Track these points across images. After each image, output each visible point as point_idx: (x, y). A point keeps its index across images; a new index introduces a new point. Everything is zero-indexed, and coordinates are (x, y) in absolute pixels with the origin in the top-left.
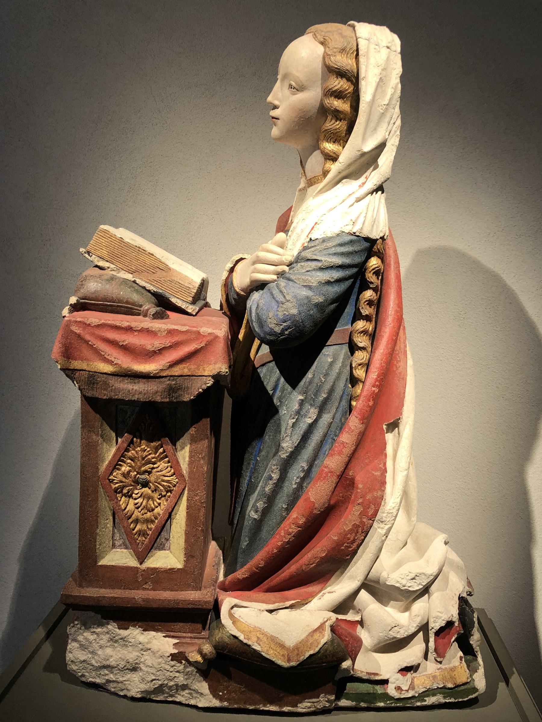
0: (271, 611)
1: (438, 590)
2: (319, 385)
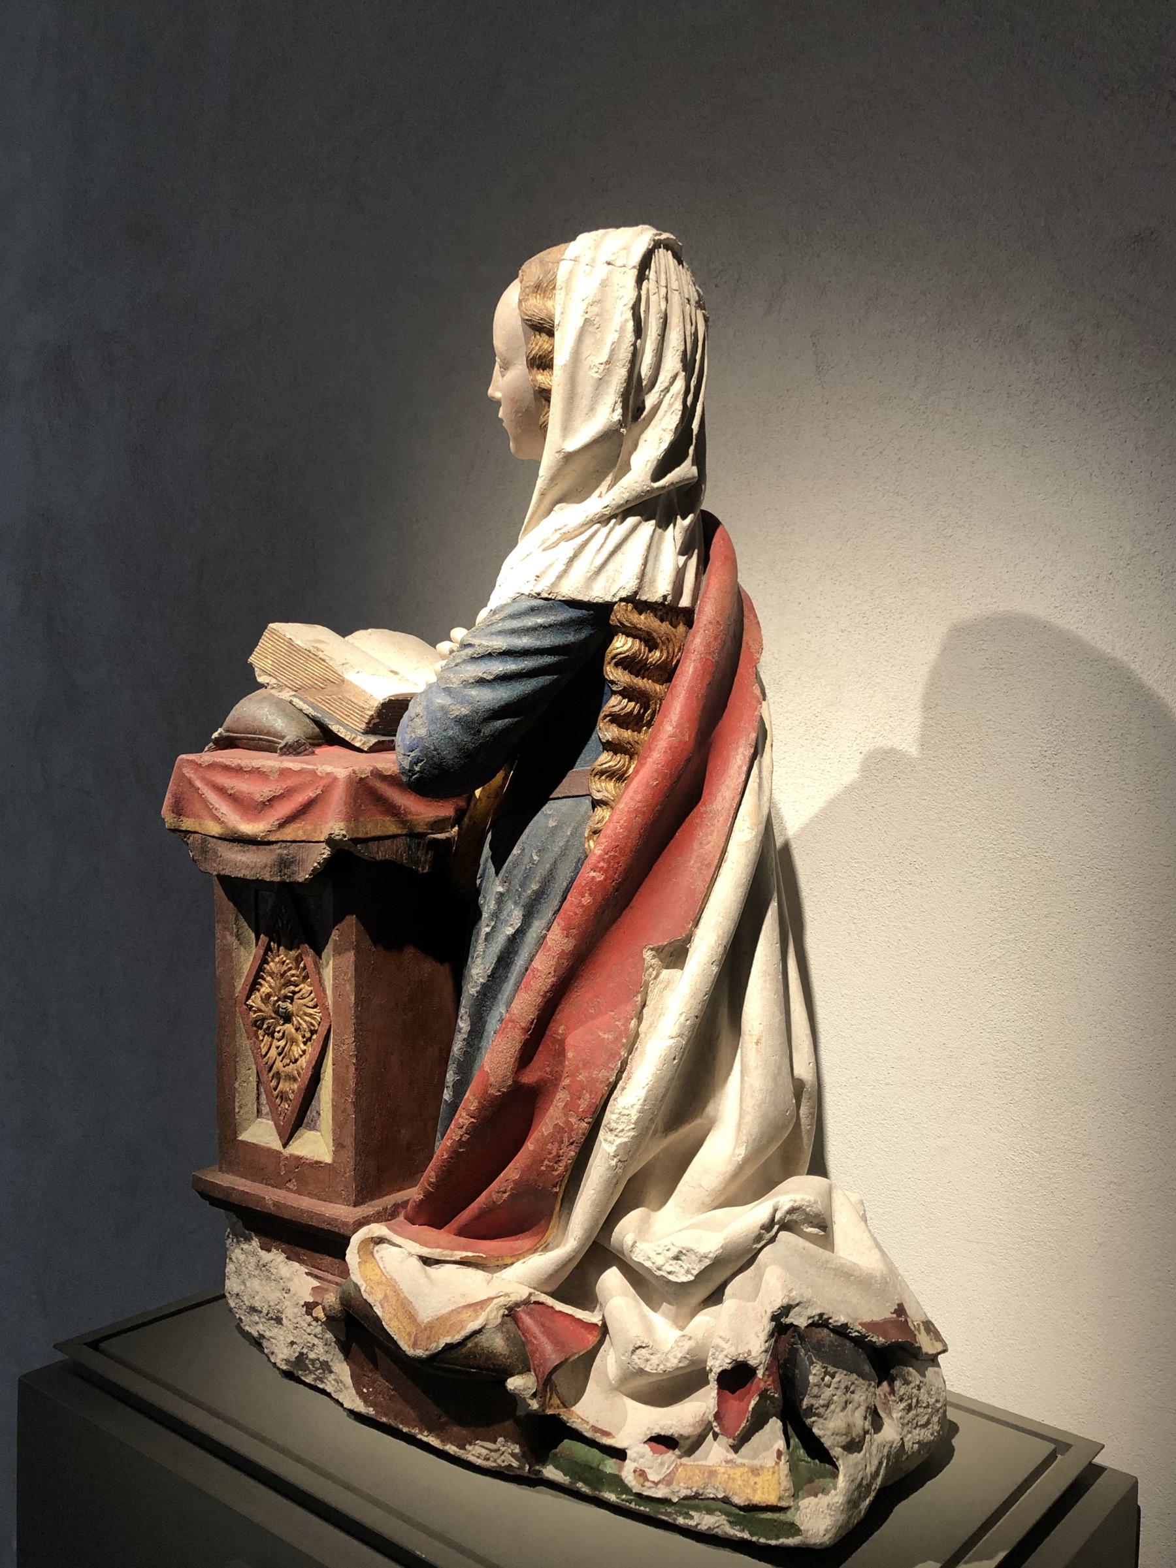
0: (427, 1261)
1: (734, 1296)
2: (528, 867)
